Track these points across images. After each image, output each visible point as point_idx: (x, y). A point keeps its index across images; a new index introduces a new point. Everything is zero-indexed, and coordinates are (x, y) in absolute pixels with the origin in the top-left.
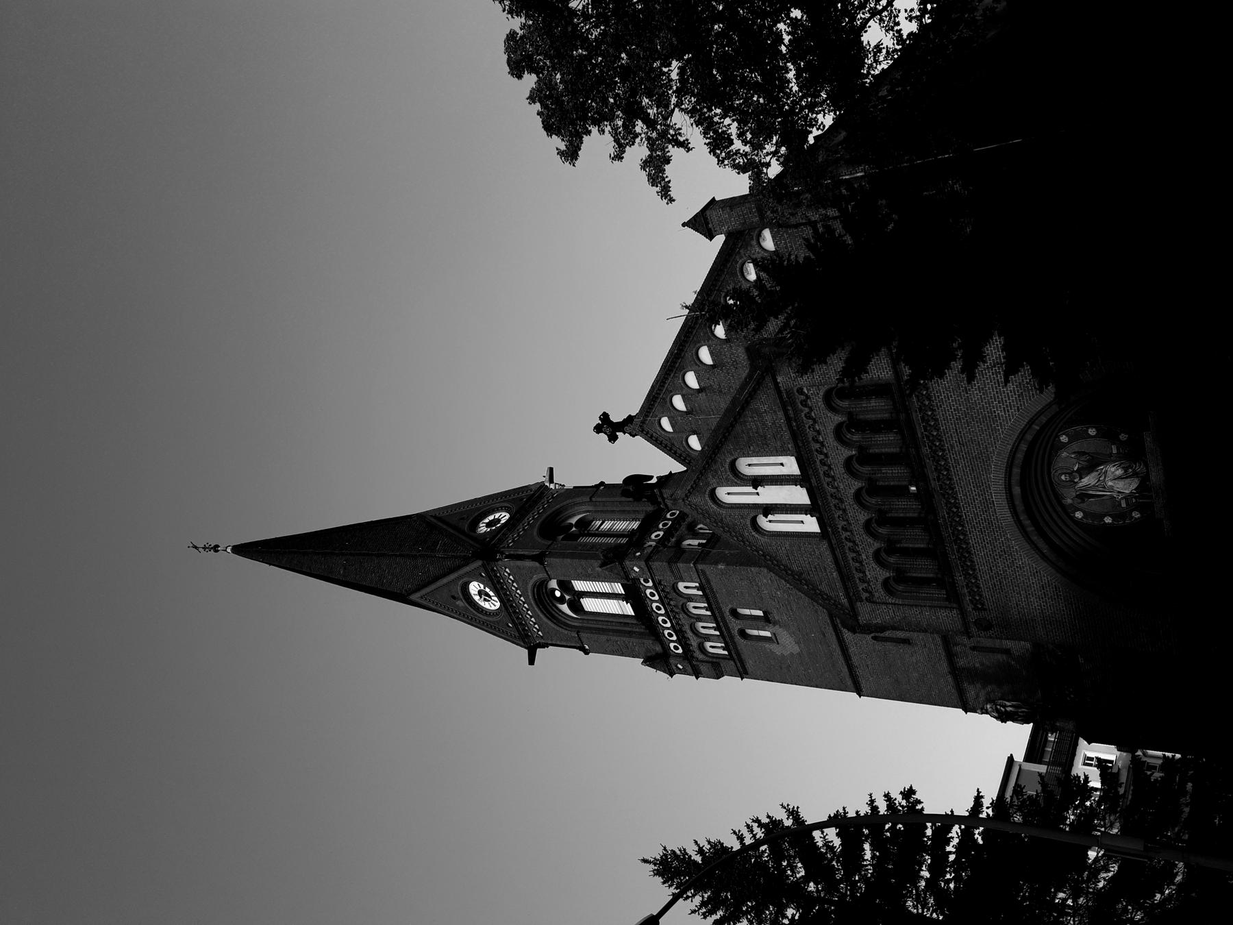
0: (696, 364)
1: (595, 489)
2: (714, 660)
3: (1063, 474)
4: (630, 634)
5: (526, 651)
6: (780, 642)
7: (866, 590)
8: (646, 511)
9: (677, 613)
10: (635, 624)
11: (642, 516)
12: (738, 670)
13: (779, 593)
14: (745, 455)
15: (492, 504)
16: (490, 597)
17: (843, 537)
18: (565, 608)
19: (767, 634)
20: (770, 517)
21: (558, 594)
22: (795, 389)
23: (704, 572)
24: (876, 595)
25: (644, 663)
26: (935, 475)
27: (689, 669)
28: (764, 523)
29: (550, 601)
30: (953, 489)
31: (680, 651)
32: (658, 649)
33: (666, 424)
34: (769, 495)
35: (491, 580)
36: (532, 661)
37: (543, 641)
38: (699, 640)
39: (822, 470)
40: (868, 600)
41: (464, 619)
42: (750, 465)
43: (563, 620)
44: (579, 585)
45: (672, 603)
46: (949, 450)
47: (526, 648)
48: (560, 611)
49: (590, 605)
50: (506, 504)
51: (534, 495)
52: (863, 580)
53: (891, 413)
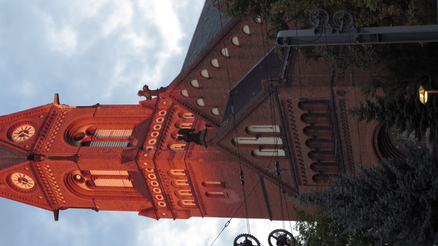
0: (209, 66)
1: (94, 109)
2: (187, 209)
3: (393, 132)
4: (131, 198)
5: (53, 212)
6: (229, 197)
7: (304, 180)
8: (135, 124)
9: (167, 186)
10: (133, 192)
11: (132, 126)
12: (201, 213)
13: (233, 173)
14: (252, 125)
15: (20, 119)
16: (27, 181)
17: (298, 159)
18: (83, 186)
19: (222, 193)
20: (262, 150)
21: (78, 177)
22: (286, 100)
23: (189, 164)
24: (309, 182)
25: (140, 214)
26: (344, 135)
27: (170, 214)
28: (257, 152)
29: (74, 182)
30: (350, 140)
31: (165, 205)
32: (150, 205)
33: (185, 93)
34: (262, 141)
35: (34, 171)
36: (57, 219)
37: (65, 206)
38: (179, 199)
39: (292, 132)
40: (305, 184)
41: (21, 200)
42: (254, 128)
43: (82, 192)
44: (94, 172)
45: (165, 181)
46: (350, 126)
47: (52, 211)
48: (81, 188)
49: (99, 182)
50: (30, 120)
51: (49, 113)
52: (303, 176)
53: (328, 111)
